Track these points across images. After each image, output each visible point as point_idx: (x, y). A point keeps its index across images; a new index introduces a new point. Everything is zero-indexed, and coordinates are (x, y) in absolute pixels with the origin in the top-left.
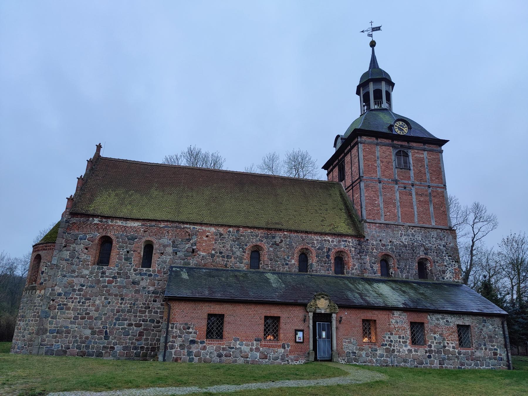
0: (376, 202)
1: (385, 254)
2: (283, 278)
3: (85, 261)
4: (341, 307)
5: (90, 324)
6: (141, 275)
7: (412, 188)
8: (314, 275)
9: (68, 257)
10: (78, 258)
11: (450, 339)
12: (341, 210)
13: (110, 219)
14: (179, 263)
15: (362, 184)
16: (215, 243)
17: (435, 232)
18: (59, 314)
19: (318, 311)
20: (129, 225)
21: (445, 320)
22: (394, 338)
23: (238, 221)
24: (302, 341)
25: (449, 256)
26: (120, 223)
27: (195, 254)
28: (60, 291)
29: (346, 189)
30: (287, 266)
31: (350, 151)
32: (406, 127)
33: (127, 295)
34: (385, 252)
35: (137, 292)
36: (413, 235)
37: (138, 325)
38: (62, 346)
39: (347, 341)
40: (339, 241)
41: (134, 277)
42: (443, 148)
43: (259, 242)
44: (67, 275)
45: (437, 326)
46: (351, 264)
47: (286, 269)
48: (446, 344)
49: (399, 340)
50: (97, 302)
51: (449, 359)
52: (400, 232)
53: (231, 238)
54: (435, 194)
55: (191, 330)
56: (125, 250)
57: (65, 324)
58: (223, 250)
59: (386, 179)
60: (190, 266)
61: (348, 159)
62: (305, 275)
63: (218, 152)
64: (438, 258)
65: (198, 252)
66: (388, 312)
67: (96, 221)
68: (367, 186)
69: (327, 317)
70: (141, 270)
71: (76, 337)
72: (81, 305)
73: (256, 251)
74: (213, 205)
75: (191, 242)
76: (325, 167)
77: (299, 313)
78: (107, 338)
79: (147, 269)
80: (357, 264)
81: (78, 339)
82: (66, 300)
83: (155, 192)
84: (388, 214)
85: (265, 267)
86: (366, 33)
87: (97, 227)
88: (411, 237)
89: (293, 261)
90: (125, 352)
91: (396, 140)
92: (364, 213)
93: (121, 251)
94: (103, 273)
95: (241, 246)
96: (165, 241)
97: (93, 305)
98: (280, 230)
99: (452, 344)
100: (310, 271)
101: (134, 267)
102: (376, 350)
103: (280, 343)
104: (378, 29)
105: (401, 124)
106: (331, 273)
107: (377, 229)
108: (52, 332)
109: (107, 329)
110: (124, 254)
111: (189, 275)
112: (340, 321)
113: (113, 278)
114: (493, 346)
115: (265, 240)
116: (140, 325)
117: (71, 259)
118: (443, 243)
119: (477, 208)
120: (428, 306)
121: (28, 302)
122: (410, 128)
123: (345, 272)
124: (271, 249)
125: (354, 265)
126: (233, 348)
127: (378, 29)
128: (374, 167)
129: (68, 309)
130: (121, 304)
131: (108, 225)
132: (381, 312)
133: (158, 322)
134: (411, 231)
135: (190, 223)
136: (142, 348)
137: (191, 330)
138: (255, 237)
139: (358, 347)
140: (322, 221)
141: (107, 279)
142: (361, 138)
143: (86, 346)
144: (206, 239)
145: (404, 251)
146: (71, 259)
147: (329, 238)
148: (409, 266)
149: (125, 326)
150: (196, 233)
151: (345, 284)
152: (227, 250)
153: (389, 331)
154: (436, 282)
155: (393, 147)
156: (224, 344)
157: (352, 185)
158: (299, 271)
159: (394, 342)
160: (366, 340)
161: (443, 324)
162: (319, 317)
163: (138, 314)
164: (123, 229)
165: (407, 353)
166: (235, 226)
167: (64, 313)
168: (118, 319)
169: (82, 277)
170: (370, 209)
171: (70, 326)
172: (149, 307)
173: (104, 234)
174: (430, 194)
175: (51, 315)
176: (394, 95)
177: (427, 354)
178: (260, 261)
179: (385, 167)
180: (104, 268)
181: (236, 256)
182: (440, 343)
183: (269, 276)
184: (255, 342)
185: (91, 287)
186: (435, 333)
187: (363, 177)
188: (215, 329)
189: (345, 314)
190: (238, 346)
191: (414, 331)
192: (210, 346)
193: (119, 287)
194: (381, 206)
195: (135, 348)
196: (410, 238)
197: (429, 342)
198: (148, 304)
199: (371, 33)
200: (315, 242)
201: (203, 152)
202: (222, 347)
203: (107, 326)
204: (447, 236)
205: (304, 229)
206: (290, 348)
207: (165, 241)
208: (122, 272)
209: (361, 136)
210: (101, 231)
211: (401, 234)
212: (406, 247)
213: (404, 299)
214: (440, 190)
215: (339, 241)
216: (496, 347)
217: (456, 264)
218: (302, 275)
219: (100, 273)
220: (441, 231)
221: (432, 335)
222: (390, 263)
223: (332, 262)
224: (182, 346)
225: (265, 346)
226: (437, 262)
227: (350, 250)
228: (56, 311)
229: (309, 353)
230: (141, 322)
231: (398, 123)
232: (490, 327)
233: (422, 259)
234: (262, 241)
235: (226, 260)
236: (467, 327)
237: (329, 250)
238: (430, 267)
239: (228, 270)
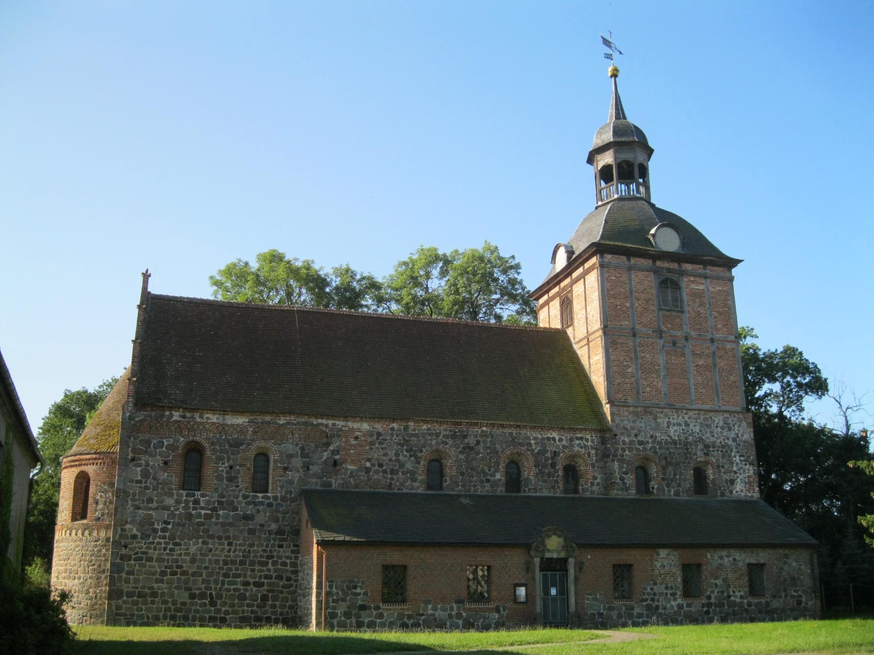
0: (628, 371)
1: (643, 458)
3: (165, 483)
4: (582, 546)
5: (186, 582)
9: (139, 478)
11: (737, 586)
13: (197, 412)
16: (371, 449)
17: (722, 418)
18: (137, 567)
19: (548, 555)
21: (731, 559)
25: (740, 456)
27: (338, 468)
30: (488, 485)
39: (590, 597)
41: (244, 508)
42: (735, 271)
43: (442, 445)
44: (141, 505)
47: (486, 488)
48: (732, 593)
52: (667, 419)
53: (395, 439)
55: (358, 590)
56: (226, 464)
59: (644, 330)
65: (344, 465)
72: (168, 554)
73: (436, 460)
75: (331, 448)
79: (264, 494)
81: (171, 606)
82: (144, 546)
87: (179, 427)
89: (498, 476)
93: (220, 465)
94: (196, 502)
95: (413, 453)
96: (289, 447)
99: (740, 591)
101: (243, 492)
108: (130, 595)
109: (212, 591)
110: (225, 470)
112: (581, 569)
113: (212, 510)
114: (796, 591)
115: (450, 442)
116: (262, 585)
117: (144, 481)
123: (580, 490)
124: (462, 457)
125: (595, 478)
126: (423, 615)
129: (150, 559)
130: (229, 551)
131: (196, 423)
133: (289, 579)
137: (358, 590)
138: (434, 437)
139: (607, 605)
141: (203, 512)
145: (672, 451)
146: (144, 481)
150: (338, 433)
153: (652, 580)
155: (654, 273)
158: (507, 491)
159: (658, 595)
161: (729, 564)
162: (548, 565)
165: (676, 609)
167: (144, 566)
168: (226, 575)
170: (620, 381)
171: (156, 585)
174: (714, 353)
177: (705, 609)
179: (643, 309)
180: (196, 494)
181: (406, 470)
182: (723, 592)
184: (455, 606)
186: (716, 578)
190: (430, 612)
192: (389, 612)
193: (224, 525)
196: (683, 430)
197: (707, 591)
198: (271, 551)
200: (533, 442)
202: (407, 613)
203: (211, 585)
204: (738, 423)
206: (507, 611)
215: (571, 440)
216: (800, 593)
219: (191, 503)
220: (730, 415)
223: (560, 474)
226: (723, 467)
227: (589, 454)
228: (132, 562)
230: (263, 580)
232: (794, 564)
233: (701, 462)
235: (390, 476)
237: (555, 454)
238: (711, 475)
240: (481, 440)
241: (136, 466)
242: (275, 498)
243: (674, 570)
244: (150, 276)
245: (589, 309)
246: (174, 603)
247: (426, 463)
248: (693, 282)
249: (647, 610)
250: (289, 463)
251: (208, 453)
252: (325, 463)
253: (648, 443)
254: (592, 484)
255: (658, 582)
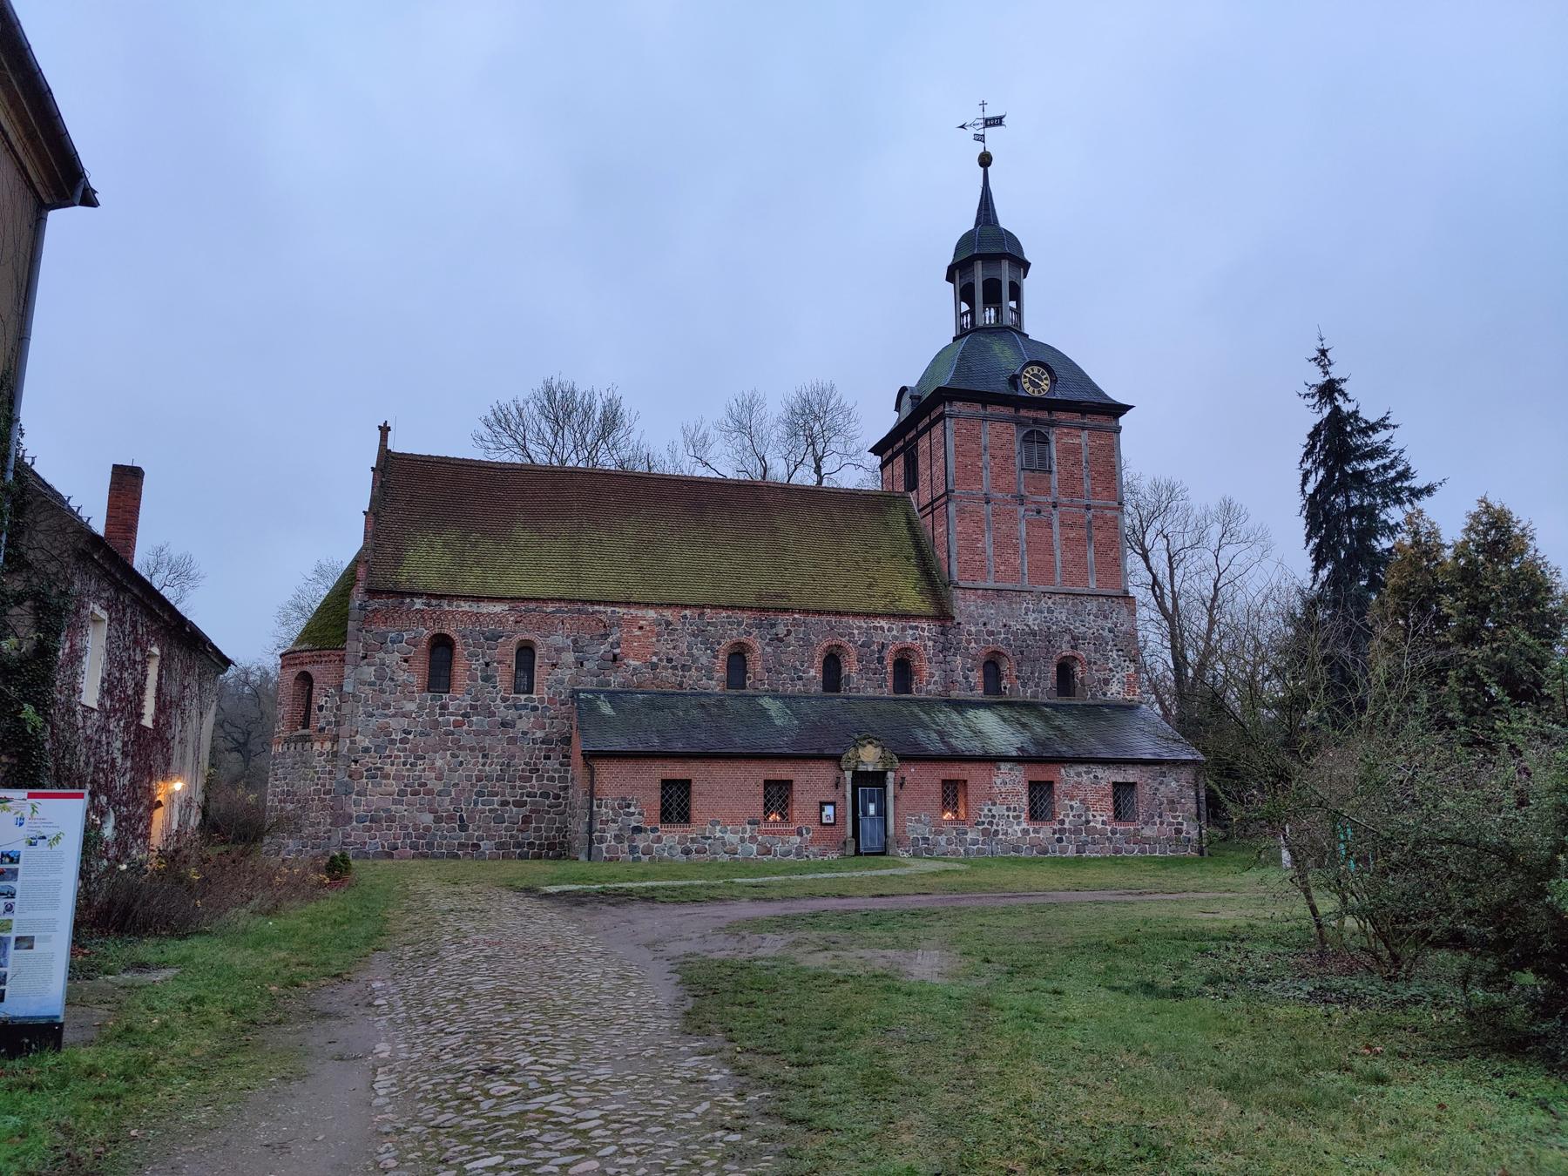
2: (794, 706)
3: (405, 685)
4: (904, 758)
6: (517, 709)
7: (1054, 512)
8: (854, 698)
9: (373, 679)
10: (392, 679)
12: (908, 559)
14: (590, 682)
15: (952, 507)
17: (1095, 603)
18: (370, 786)
19: (861, 768)
20: (485, 611)
21: (1091, 776)
23: (699, 596)
24: (832, 821)
25: (1118, 651)
26: (465, 606)
27: (618, 663)
28: (367, 743)
29: (920, 511)
30: (801, 682)
31: (929, 428)
32: (1046, 379)
33: (493, 749)
34: (992, 647)
35: (512, 741)
36: (1050, 611)
37: (520, 804)
38: (383, 845)
40: (904, 629)
41: (503, 712)
42: (1122, 420)
44: (375, 712)
45: (1077, 786)
46: (925, 673)
48: (1091, 818)
49: (1007, 814)
50: (439, 763)
51: (1094, 842)
52: (1025, 605)
54: (1100, 522)
55: (632, 809)
57: (382, 804)
58: (674, 654)
59: (1000, 495)
60: (611, 688)
61: (923, 444)
62: (835, 697)
63: (615, 387)
64: (1098, 655)
66: (989, 766)
67: (419, 604)
68: (961, 511)
69: (878, 778)
70: (515, 699)
71: (407, 827)
72: (408, 770)
74: (645, 559)
75: (610, 640)
76: (877, 450)
77: (826, 771)
78: (463, 828)
80: (937, 673)
83: (522, 534)
84: (1002, 568)
85: (758, 684)
86: (971, 131)
87: (423, 617)
88: (1046, 614)
89: (812, 672)
90: (501, 852)
91: (1025, 407)
92: (954, 568)
94: (444, 707)
95: (709, 645)
96: (558, 639)
97: (432, 768)
98: (786, 610)
100: (845, 690)
102: (966, 833)
104: (997, 121)
105: (1036, 372)
106: (887, 691)
107: (979, 601)
108: (360, 820)
111: (613, 708)
112: (901, 785)
113: (463, 715)
114: (1174, 817)
115: (755, 632)
116: (524, 804)
117: (378, 683)
119: (1227, 507)
120: (1064, 750)
121: (297, 766)
122: (1054, 381)
124: (768, 649)
125: (931, 675)
126: (710, 838)
127: (997, 121)
128: (977, 470)
129: (387, 776)
130: (484, 765)
132: (976, 766)
133: (557, 797)
134: (1047, 603)
135: (606, 603)
136: (531, 844)
137: (632, 809)
140: (870, 586)
141: (452, 718)
142: (951, 406)
143: (427, 843)
144: (639, 633)
146: (378, 683)
147: (883, 623)
148: (1040, 673)
149: (496, 806)
150: (619, 623)
151: (912, 713)
152: (682, 654)
154: (1091, 702)
155: (1017, 424)
156: (692, 831)
157: (931, 504)
158: (825, 689)
160: (948, 815)
162: (861, 778)
163: (518, 783)
164: (474, 618)
165: (1019, 835)
166: (695, 606)
168: (480, 794)
169: (404, 716)
172: (538, 770)
173: (437, 631)
174: (1090, 522)
175: (356, 789)
176: (1028, 285)
177: (1056, 836)
178: (747, 672)
182: (1080, 816)
183: (766, 702)
184: (748, 827)
185: (422, 734)
186: (1071, 799)
187: (953, 491)
188: (674, 805)
189: (911, 771)
190: (718, 835)
191: (1035, 797)
193: (477, 734)
194: (988, 551)
195: (519, 845)
198: (535, 764)
199: (981, 132)
200: (856, 632)
201: (581, 389)
205: (832, 607)
207: (558, 639)
208: (479, 703)
209: (951, 400)
210: (430, 624)
211: (1027, 609)
212: (1035, 635)
213: (1021, 739)
214: (1109, 513)
215: (904, 629)
216: (1180, 820)
217: (1132, 665)
218: (831, 698)
221: (1066, 802)
222: (1002, 668)
224: (618, 838)
225: (766, 832)
226: (1095, 663)
227: (925, 646)
228: (364, 780)
229: (845, 843)
230: (525, 798)
231: (1029, 369)
232: (1173, 784)
234: (751, 634)
236: (1132, 786)
239: (685, 694)
240: (792, 629)
241: (369, 665)
242: (541, 700)
243: (1019, 788)
244: (389, 429)
245: (934, 470)
246: (416, 829)
247: (726, 657)
248: (1067, 434)
249: (983, 835)
250: (560, 658)
251: (459, 648)
252: (602, 658)
253: (1000, 633)
254: (929, 683)
255: (998, 802)
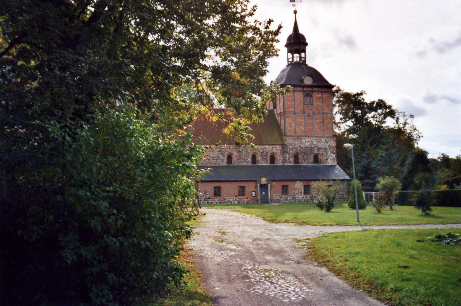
19: (262, 183)
22: (296, 192)
46: (278, 159)
55: (207, 194)
89: (249, 160)
95: (223, 154)
103: (245, 197)
115: (234, 150)
118: (328, 144)
137: (207, 194)
162: (262, 186)
184: (235, 197)
190: (228, 199)
215: (272, 148)
224: (205, 200)
227: (278, 152)
237: (267, 152)
